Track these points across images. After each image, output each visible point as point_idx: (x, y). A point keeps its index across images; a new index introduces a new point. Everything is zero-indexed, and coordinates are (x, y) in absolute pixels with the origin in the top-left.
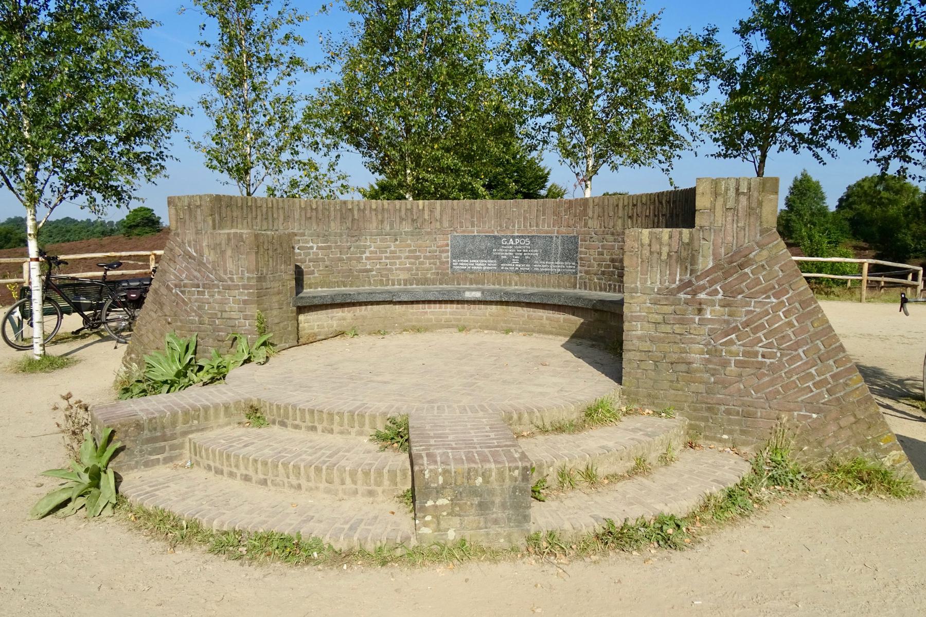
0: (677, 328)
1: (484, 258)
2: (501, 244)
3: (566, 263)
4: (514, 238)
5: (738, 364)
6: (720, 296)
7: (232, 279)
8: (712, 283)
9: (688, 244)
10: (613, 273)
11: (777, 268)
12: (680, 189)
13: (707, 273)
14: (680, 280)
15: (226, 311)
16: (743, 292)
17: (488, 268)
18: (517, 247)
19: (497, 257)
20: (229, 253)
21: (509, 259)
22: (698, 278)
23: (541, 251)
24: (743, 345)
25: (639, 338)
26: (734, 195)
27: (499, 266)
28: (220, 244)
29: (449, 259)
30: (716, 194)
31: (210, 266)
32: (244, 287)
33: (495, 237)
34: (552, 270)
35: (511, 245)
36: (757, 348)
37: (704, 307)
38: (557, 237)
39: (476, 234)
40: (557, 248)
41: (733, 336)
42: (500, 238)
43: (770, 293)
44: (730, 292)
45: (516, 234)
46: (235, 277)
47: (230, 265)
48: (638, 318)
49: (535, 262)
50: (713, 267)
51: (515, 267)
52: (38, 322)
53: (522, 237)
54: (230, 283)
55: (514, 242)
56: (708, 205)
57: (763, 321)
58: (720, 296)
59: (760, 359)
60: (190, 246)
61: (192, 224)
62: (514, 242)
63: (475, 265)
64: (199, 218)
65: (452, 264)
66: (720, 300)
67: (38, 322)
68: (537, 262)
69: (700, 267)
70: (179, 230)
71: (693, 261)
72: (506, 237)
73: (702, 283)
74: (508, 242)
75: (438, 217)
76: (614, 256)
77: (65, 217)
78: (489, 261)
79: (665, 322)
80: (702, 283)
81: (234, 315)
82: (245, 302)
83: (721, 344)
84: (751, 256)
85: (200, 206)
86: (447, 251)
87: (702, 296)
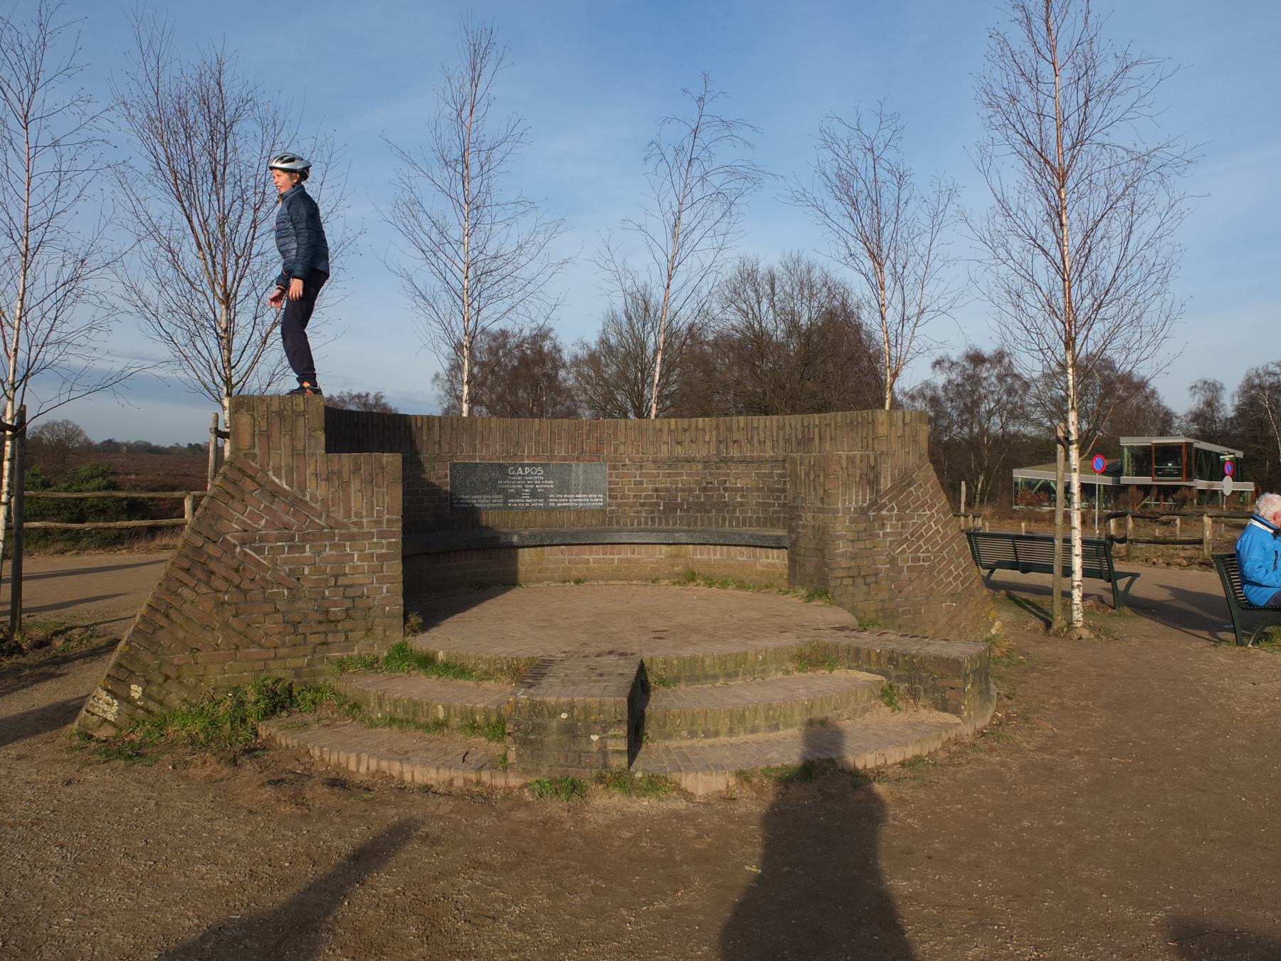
0: (868, 544)
1: (487, 493)
2: (507, 474)
3: (590, 496)
4: (523, 466)
5: (910, 569)
6: (895, 512)
8: (890, 501)
9: (874, 468)
10: (658, 504)
11: (929, 486)
13: (887, 493)
14: (870, 499)
15: (345, 575)
16: (910, 507)
17: (493, 505)
18: (527, 478)
20: (355, 485)
22: (881, 497)
24: (911, 553)
26: (902, 425)
27: (506, 502)
28: (340, 472)
30: (891, 425)
31: (318, 506)
32: (382, 535)
33: (500, 465)
34: (572, 504)
35: (520, 475)
36: (919, 554)
37: (885, 522)
39: (478, 461)
40: (578, 477)
41: (905, 546)
42: (507, 467)
43: (926, 507)
44: (902, 508)
45: (527, 462)
46: (365, 520)
47: (356, 502)
48: (839, 537)
50: (891, 487)
51: (525, 503)
52: (1075, 528)
53: (534, 465)
54: (355, 530)
55: (524, 472)
56: (885, 432)
57: (922, 530)
58: (895, 512)
59: (921, 563)
60: (278, 476)
61: (286, 440)
62: (524, 472)
64: (301, 431)
65: (451, 501)
66: (896, 515)
67: (1075, 528)
69: (882, 487)
70: (257, 450)
71: (878, 483)
72: (513, 465)
73: (883, 501)
74: (516, 472)
75: (437, 438)
76: (658, 486)
79: (858, 540)
80: (883, 501)
81: (360, 579)
82: (381, 557)
84: (914, 476)
85: (303, 413)
87: (884, 512)
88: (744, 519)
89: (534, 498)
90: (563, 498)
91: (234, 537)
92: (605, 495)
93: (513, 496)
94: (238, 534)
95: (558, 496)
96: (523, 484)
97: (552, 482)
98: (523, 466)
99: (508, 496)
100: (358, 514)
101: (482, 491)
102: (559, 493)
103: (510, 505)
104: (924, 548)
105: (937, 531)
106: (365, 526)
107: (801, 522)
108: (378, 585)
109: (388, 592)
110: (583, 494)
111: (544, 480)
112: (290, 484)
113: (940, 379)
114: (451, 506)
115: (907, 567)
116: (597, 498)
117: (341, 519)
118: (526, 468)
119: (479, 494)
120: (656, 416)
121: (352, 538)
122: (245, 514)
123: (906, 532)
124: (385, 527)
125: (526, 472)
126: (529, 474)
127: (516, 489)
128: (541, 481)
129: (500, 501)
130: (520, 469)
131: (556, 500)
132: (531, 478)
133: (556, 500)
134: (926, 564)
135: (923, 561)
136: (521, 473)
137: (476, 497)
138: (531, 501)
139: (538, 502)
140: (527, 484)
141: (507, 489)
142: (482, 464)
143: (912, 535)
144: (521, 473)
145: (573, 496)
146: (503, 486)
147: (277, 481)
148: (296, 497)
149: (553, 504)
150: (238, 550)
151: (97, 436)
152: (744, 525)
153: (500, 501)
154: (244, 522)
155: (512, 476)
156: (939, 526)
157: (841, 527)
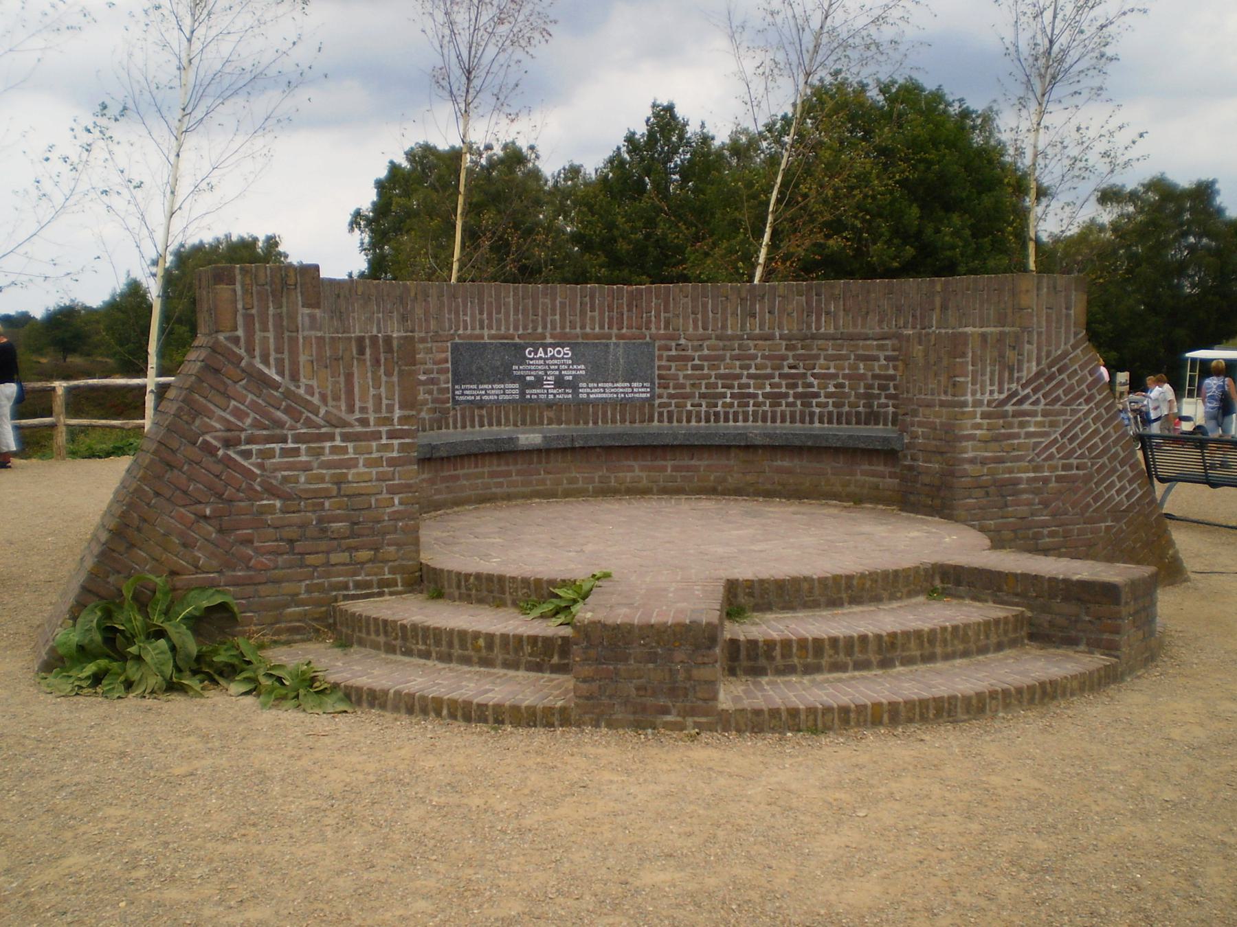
3: (634, 385)
4: (545, 347)
7: (364, 422)
12: (289, 260)
19: (521, 379)
21: (539, 382)
23: (590, 366)
25: (972, 461)
27: (523, 394)
29: (450, 385)
33: (515, 345)
34: (611, 396)
35: (541, 358)
38: (616, 345)
45: (549, 341)
49: (581, 385)
51: (548, 394)
55: (546, 353)
60: (266, 361)
62: (546, 353)
63: (486, 394)
65: (453, 392)
68: (584, 385)
77: (24, 310)
78: (507, 386)
82: (392, 462)
83: (1043, 460)
86: (447, 371)
88: (839, 415)
89: (560, 388)
90: (598, 387)
91: (215, 438)
92: (653, 383)
93: (532, 385)
94: (219, 434)
95: (591, 385)
96: (545, 370)
97: (583, 367)
98: (545, 347)
99: (525, 385)
100: (363, 410)
101: (492, 379)
102: (593, 381)
103: (528, 396)
104: (1079, 452)
105: (1096, 432)
106: (372, 423)
107: (916, 419)
108: (388, 496)
109: (400, 503)
110: (624, 381)
111: (573, 364)
112: (281, 373)
113: (1106, 216)
114: (454, 398)
115: (1056, 476)
116: (643, 387)
117: (344, 415)
118: (549, 349)
119: (488, 383)
120: (460, 279)
121: (355, 438)
122: (228, 410)
123: (1055, 432)
124: (751, 402)
125: (549, 355)
126: (553, 357)
127: (574, 376)
128: (569, 365)
129: (514, 392)
130: (541, 349)
131: (589, 390)
132: (556, 362)
133: (589, 390)
134: (1081, 472)
135: (1077, 468)
136: (543, 355)
137: (486, 386)
138: (555, 391)
139: (565, 393)
140: (550, 370)
141: (524, 377)
142: (492, 344)
143: (1063, 435)
144: (543, 355)
145: (610, 385)
146: (519, 373)
147: (266, 371)
148: (288, 389)
149: (585, 396)
150: (220, 453)
151: (38, 313)
152: (839, 422)
153: (514, 392)
154: (228, 421)
155: (531, 359)
156: (1099, 424)
157: (974, 425)
